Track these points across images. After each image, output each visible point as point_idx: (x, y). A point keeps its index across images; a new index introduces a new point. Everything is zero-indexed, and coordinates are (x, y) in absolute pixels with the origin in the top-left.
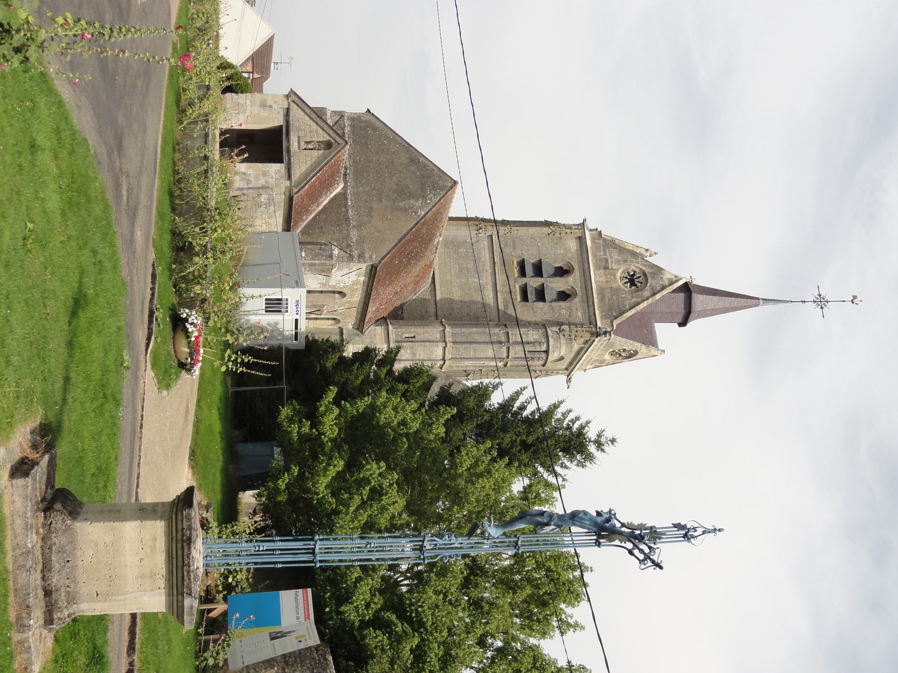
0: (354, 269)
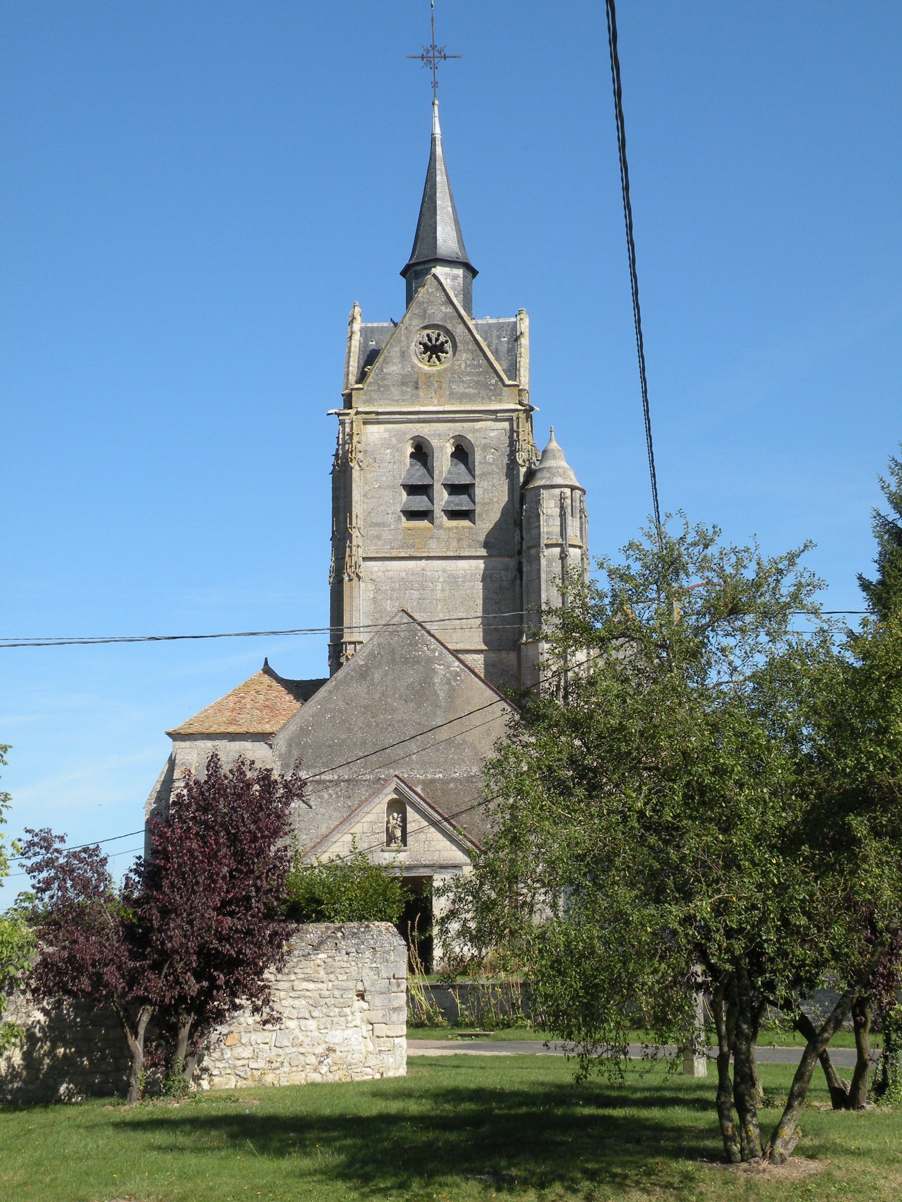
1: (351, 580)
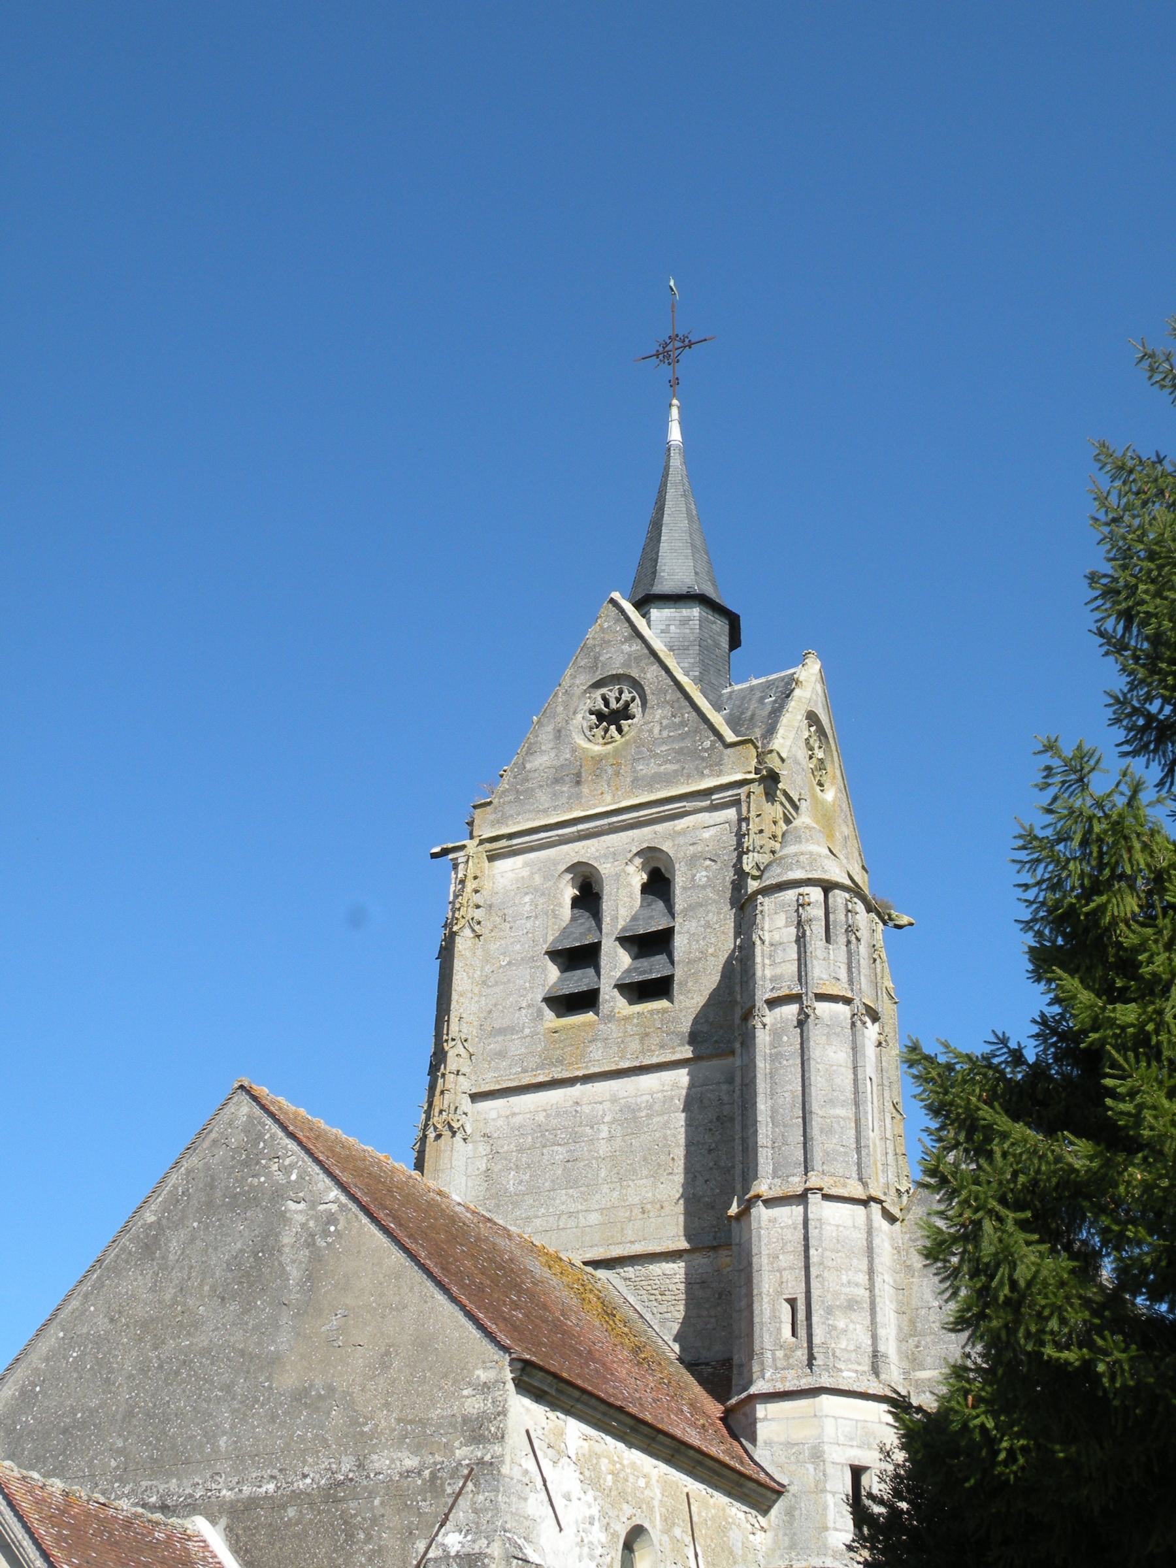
0: (530, 1464)
1: (439, 1136)
